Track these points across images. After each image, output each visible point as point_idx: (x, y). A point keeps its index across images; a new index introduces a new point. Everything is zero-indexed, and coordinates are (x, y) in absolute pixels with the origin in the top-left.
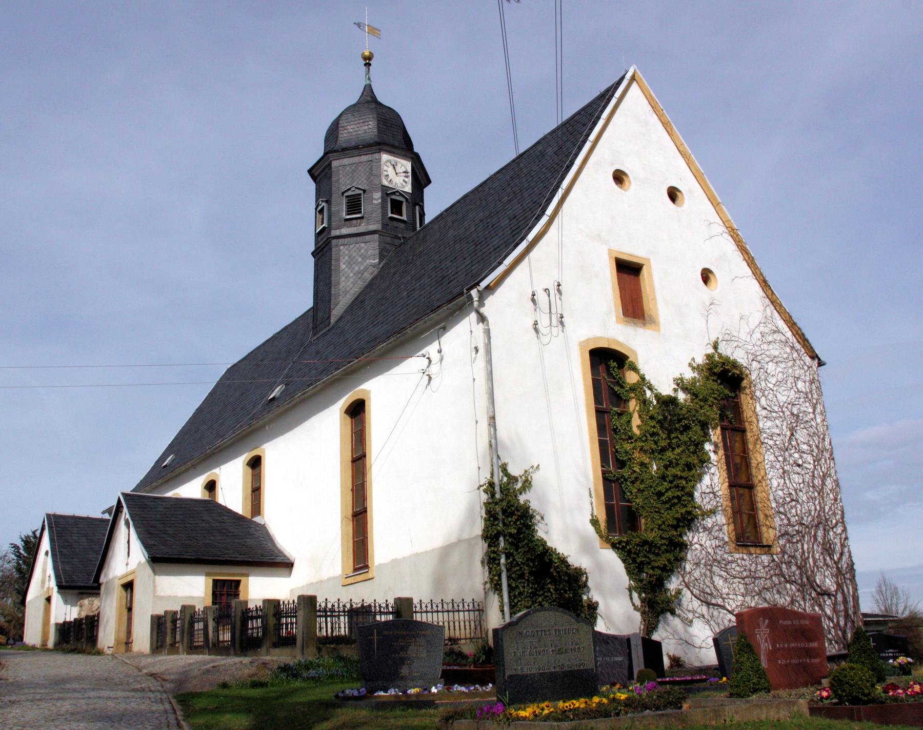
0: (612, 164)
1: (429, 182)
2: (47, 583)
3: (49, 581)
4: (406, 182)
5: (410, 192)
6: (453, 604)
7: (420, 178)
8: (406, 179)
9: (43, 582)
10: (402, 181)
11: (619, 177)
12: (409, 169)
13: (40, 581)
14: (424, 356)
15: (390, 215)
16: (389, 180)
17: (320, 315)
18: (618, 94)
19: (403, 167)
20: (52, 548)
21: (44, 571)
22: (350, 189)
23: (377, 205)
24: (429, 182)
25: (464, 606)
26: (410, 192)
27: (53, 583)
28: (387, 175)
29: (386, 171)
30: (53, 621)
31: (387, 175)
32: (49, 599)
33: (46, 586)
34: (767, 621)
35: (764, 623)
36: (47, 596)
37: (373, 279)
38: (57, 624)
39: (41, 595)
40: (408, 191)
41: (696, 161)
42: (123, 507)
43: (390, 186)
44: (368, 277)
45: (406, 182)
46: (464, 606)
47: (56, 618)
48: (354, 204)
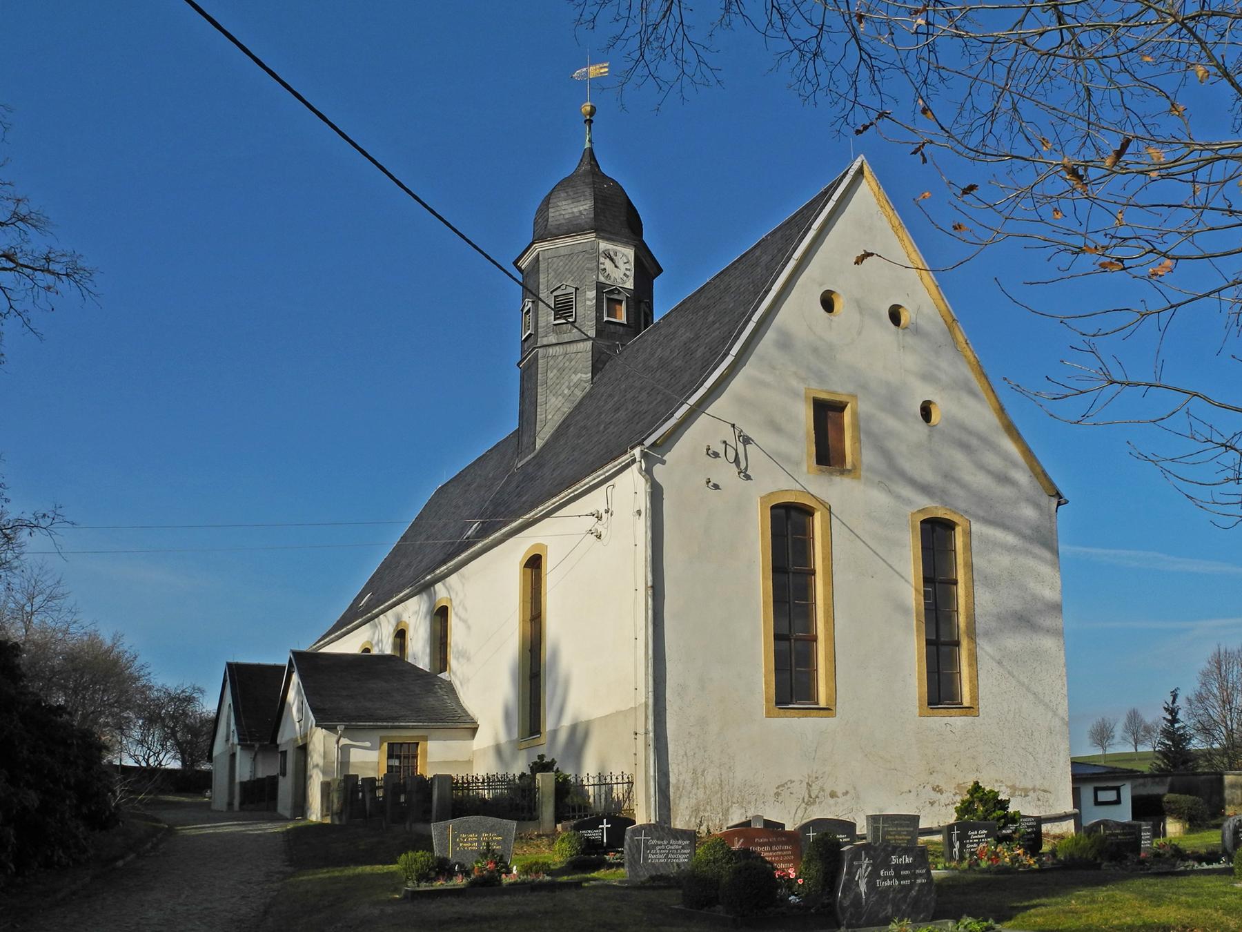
0: (821, 285)
1: (660, 271)
2: (231, 739)
3: (233, 737)
4: (627, 277)
5: (632, 288)
6: (600, 777)
7: (646, 269)
8: (628, 273)
9: (227, 740)
10: (622, 276)
11: (828, 303)
12: (632, 259)
13: (225, 734)
14: (593, 515)
15: (606, 319)
16: (606, 274)
17: (525, 439)
18: (836, 197)
19: (624, 258)
20: (233, 702)
21: (228, 725)
22: (560, 287)
23: (591, 307)
24: (660, 271)
25: (623, 779)
26: (632, 288)
27: (235, 739)
28: (605, 269)
29: (603, 264)
30: (237, 780)
31: (605, 269)
32: (233, 756)
33: (231, 741)
34: (742, 840)
35: (739, 841)
36: (231, 753)
37: (583, 398)
38: (241, 783)
39: (226, 751)
40: (629, 287)
41: (354, 624)
42: (293, 666)
43: (608, 282)
44: (579, 394)
45: (627, 277)
46: (623, 779)
47: (240, 777)
48: (563, 308)
